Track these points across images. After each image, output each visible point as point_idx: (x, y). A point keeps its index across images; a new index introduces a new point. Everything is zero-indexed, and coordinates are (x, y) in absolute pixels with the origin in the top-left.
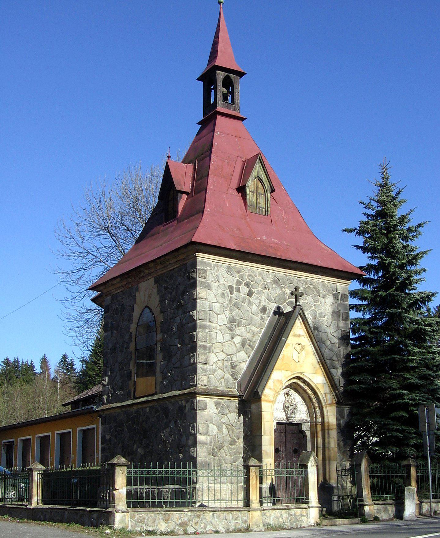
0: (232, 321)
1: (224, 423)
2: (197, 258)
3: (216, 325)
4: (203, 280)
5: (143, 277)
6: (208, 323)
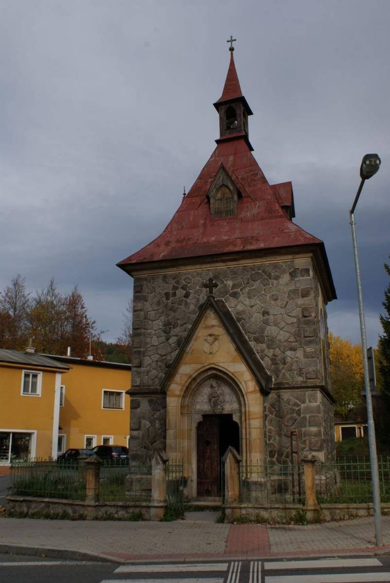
1: (157, 419)
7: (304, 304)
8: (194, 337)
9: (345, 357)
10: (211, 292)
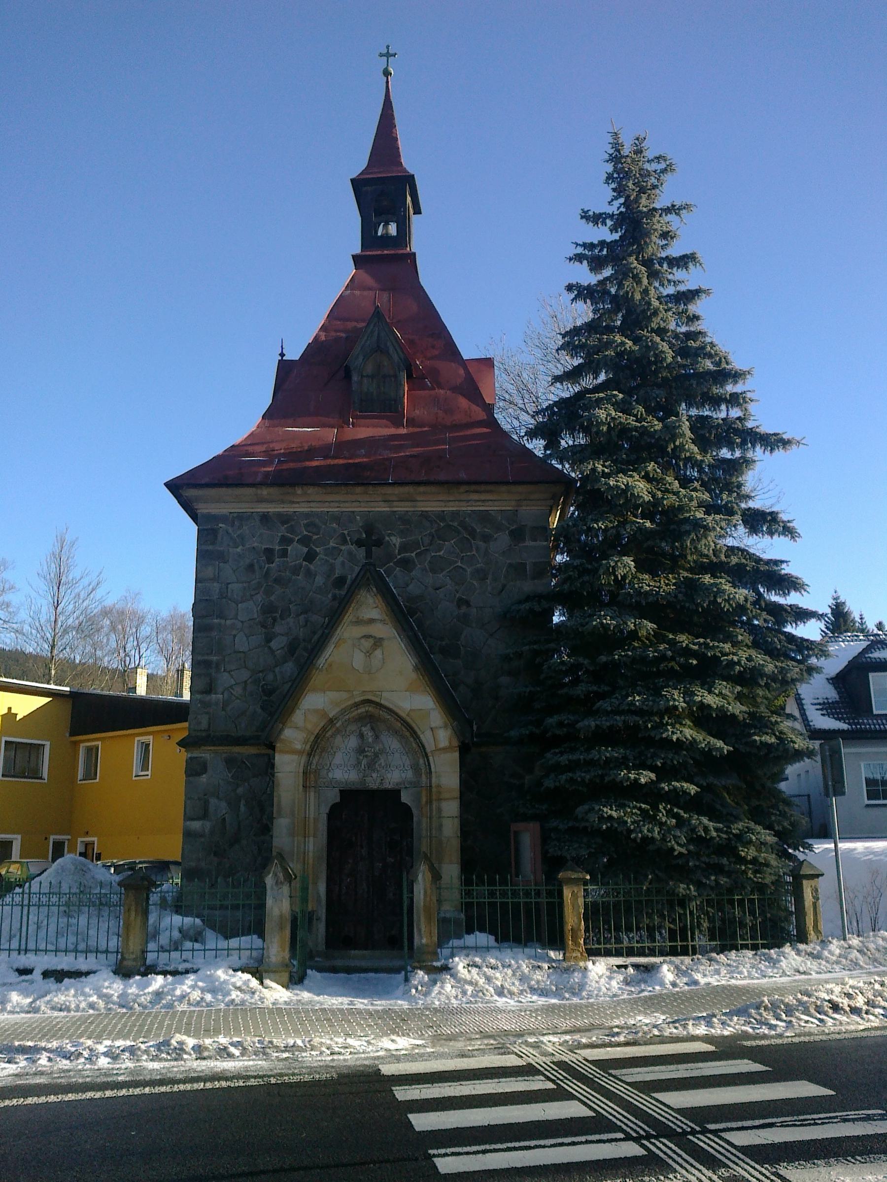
0: (268, 610)
8: (334, 640)
9: (607, 894)
10: (369, 554)
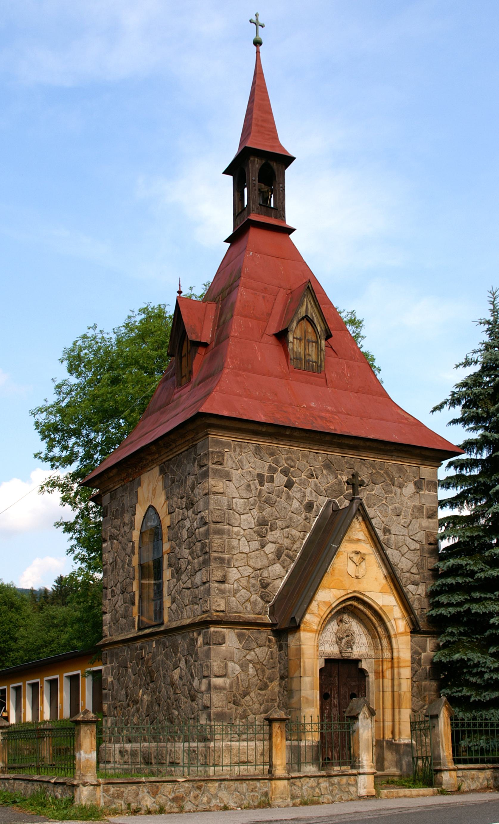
0: (262, 523)
1: (250, 661)
2: (209, 436)
3: (238, 528)
4: (218, 467)
5: (146, 466)
6: (227, 527)
7: (428, 528)
